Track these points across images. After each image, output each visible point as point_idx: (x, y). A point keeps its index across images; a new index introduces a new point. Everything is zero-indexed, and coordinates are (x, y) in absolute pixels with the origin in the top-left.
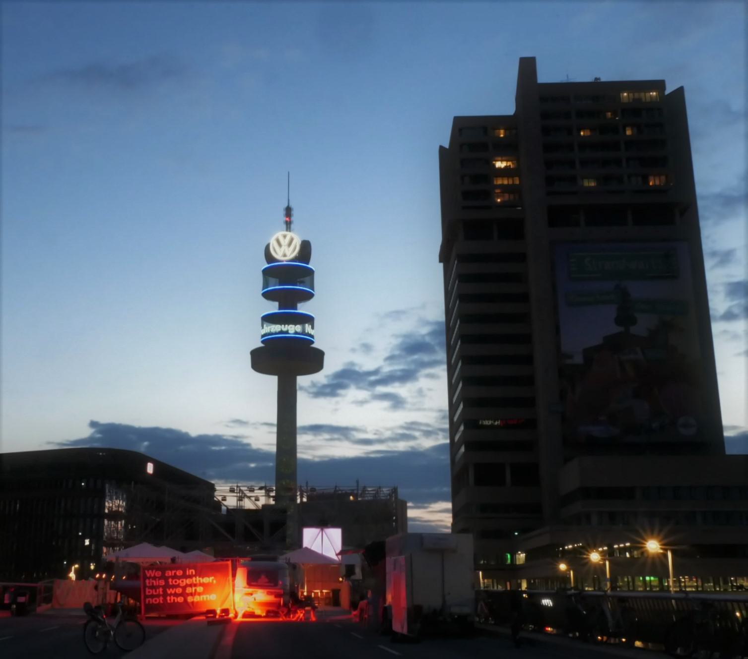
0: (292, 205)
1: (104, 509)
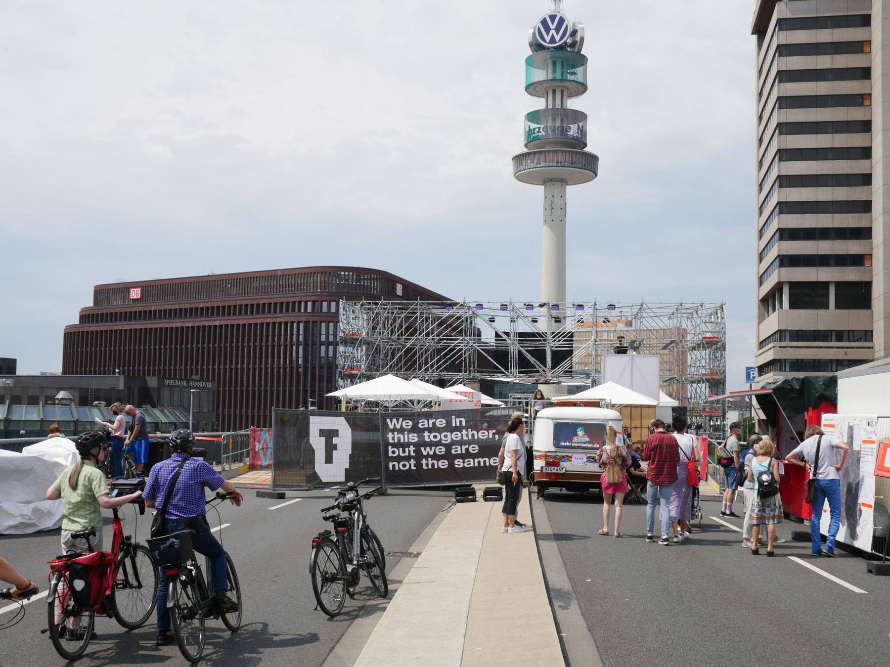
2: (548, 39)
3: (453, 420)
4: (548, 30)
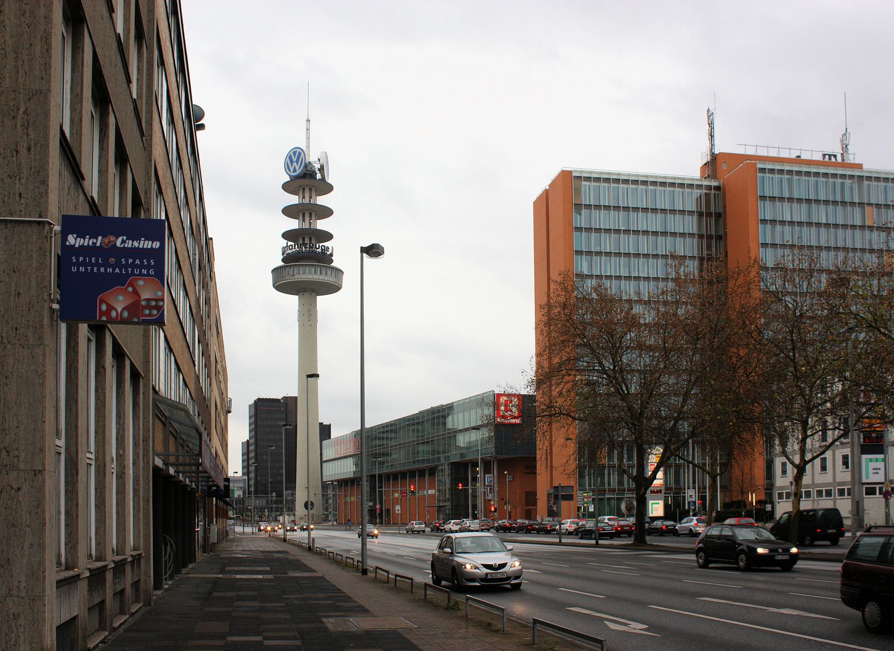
2: (292, 169)
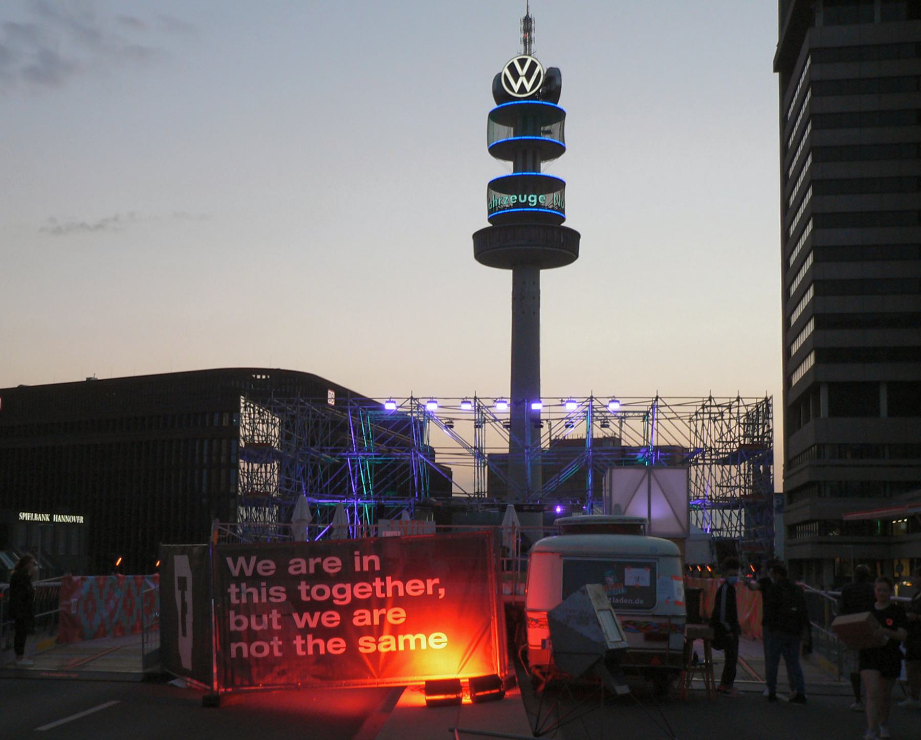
0: (532, 14)
1: (238, 441)
2: (516, 87)
3: (357, 560)
4: (516, 76)
